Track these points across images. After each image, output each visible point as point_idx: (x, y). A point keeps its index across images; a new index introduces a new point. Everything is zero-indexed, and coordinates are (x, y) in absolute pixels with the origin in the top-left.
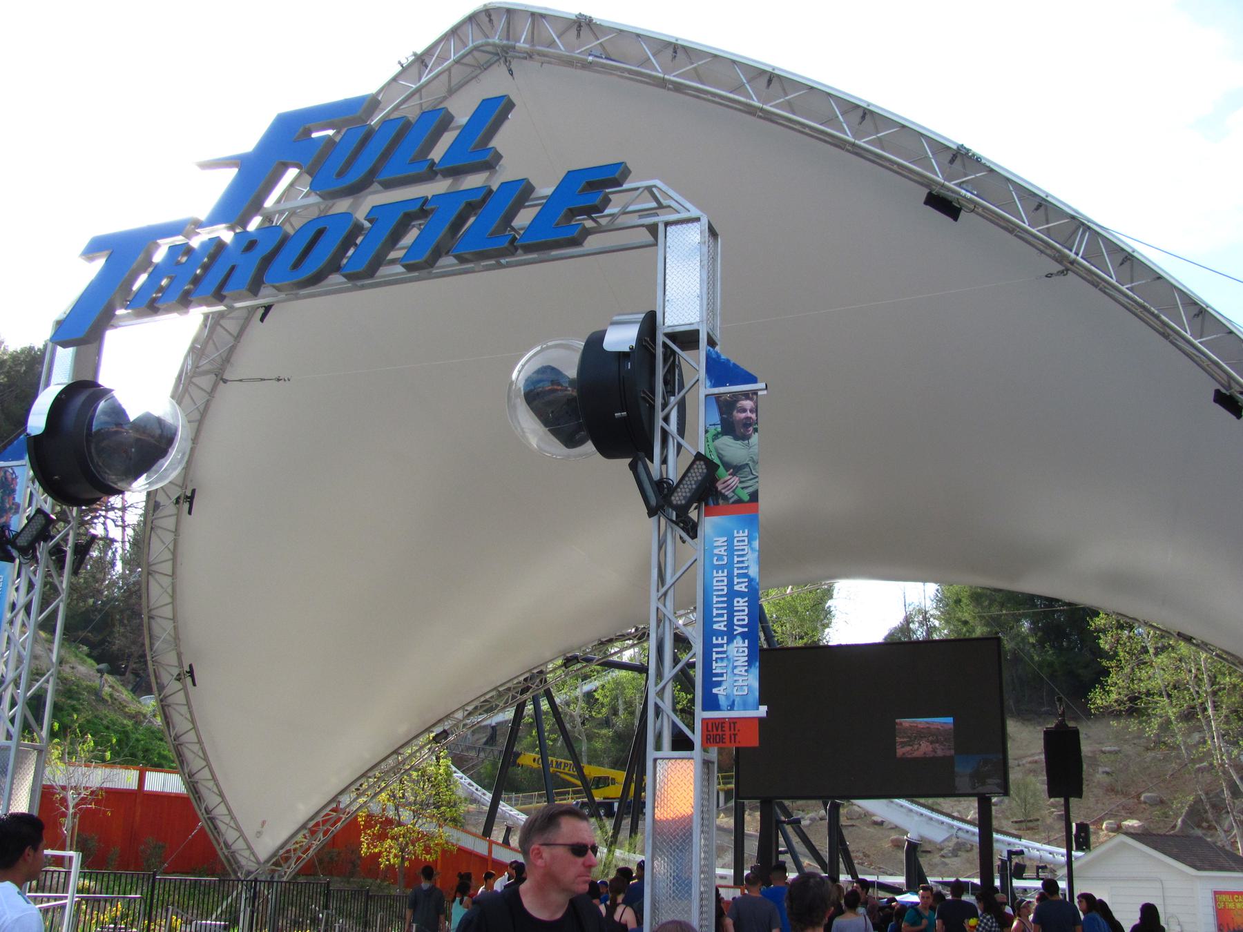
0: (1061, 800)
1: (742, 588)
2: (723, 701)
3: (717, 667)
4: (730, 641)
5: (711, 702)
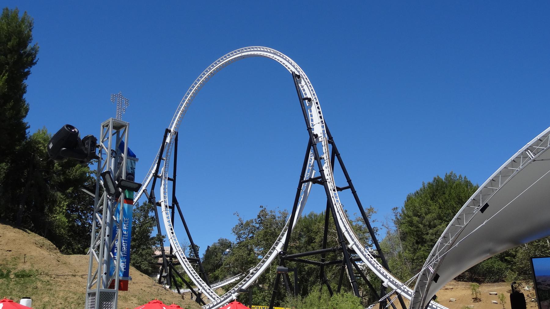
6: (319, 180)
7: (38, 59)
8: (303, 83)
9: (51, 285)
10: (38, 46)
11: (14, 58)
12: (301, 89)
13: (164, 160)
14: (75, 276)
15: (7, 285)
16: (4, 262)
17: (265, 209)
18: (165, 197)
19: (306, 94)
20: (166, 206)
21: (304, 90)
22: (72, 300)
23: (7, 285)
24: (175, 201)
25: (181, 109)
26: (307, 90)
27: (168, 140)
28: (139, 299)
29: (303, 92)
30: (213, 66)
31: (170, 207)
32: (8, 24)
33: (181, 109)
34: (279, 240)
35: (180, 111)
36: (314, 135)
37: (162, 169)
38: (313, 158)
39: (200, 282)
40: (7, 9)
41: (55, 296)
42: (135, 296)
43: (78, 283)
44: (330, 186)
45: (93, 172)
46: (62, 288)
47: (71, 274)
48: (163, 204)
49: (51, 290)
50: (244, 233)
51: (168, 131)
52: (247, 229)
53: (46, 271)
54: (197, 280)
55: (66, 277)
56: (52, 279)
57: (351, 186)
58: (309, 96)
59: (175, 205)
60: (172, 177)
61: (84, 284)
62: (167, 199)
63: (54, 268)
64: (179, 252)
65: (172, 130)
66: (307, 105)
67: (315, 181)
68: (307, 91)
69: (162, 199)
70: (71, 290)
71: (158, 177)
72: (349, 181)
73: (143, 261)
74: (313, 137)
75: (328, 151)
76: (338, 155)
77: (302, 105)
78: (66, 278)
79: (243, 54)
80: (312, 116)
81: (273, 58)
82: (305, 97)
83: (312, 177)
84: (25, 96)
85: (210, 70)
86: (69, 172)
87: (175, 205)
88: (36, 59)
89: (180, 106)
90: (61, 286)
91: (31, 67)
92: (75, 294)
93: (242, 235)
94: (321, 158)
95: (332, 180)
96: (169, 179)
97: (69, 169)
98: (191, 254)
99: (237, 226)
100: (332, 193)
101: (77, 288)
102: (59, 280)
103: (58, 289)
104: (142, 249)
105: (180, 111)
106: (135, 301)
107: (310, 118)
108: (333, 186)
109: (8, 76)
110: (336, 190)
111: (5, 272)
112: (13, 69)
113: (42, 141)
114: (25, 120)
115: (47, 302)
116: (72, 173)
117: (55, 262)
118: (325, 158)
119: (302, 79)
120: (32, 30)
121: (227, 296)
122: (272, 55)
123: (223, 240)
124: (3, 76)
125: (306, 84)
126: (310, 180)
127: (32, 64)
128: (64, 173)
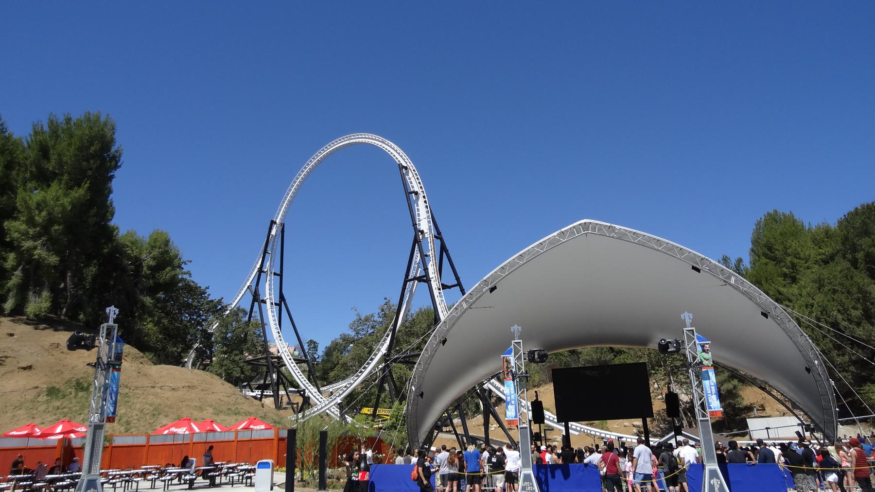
0: (538, 425)
1: (713, 384)
2: (712, 407)
3: (710, 401)
4: (712, 395)
5: (710, 408)
6: (425, 278)
7: (123, 162)
8: (410, 175)
9: (129, 397)
10: (122, 147)
11: (97, 164)
12: (409, 181)
13: (270, 254)
14: (154, 387)
15: (87, 398)
16: (86, 375)
17: (389, 301)
18: (270, 294)
19: (413, 187)
20: (272, 304)
21: (411, 183)
22: (148, 411)
23: (87, 398)
24: (282, 298)
25: (287, 199)
26: (415, 184)
27: (273, 232)
28: (214, 408)
29: (410, 185)
30: (314, 158)
31: (276, 304)
32: (91, 128)
33: (287, 199)
34: (384, 341)
35: (287, 201)
36: (420, 231)
37: (267, 264)
38: (419, 255)
39: (306, 384)
40: (89, 114)
41: (132, 408)
42: (211, 406)
43: (156, 395)
44: (435, 285)
45: (187, 273)
46: (140, 400)
47: (151, 385)
48: (268, 302)
49: (128, 402)
50: (363, 329)
51: (273, 223)
52: (366, 324)
53: (126, 384)
54: (304, 382)
55: (144, 388)
56: (131, 391)
57: (459, 284)
58: (416, 189)
59: (283, 302)
60: (279, 272)
61: (162, 396)
62: (273, 296)
63: (134, 380)
64: (285, 353)
65: (278, 221)
66: (414, 198)
67: (420, 279)
68: (414, 184)
69: (268, 296)
70: (148, 402)
71: (263, 272)
72: (457, 278)
73: (235, 367)
74: (418, 232)
75: (434, 248)
76: (447, 251)
77: (408, 199)
78: (145, 390)
79: (351, 141)
80: (418, 210)
81: (381, 147)
82: (412, 190)
83: (418, 276)
84: (111, 196)
85: (317, 157)
86: (159, 276)
87: (283, 302)
88: (121, 161)
89: (289, 191)
90: (139, 398)
91: (116, 170)
92: (151, 405)
93: (361, 332)
94: (426, 256)
95: (437, 278)
96: (275, 274)
97: (159, 273)
98: (310, 351)
99: (355, 321)
100: (436, 293)
101: (155, 399)
102: (138, 391)
103: (135, 401)
104: (234, 354)
105: (287, 201)
106: (211, 410)
107: (417, 212)
108: (438, 285)
109: (90, 183)
110: (441, 289)
111: (86, 385)
112: (96, 175)
113: (130, 244)
114: (112, 223)
115: (123, 414)
116: (162, 277)
117: (135, 374)
118: (431, 256)
119: (409, 170)
120: (115, 133)
121: (331, 400)
122: (380, 144)
123: (345, 335)
124: (85, 184)
125: (413, 176)
126: (415, 278)
127: (116, 167)
128: (154, 277)
